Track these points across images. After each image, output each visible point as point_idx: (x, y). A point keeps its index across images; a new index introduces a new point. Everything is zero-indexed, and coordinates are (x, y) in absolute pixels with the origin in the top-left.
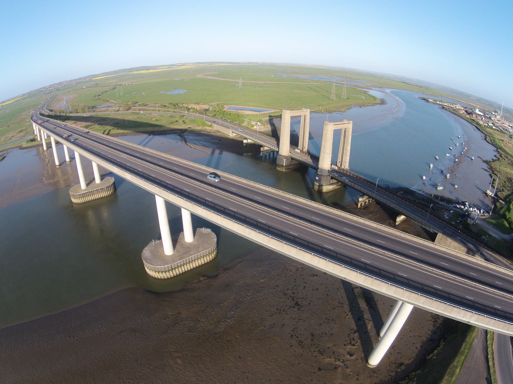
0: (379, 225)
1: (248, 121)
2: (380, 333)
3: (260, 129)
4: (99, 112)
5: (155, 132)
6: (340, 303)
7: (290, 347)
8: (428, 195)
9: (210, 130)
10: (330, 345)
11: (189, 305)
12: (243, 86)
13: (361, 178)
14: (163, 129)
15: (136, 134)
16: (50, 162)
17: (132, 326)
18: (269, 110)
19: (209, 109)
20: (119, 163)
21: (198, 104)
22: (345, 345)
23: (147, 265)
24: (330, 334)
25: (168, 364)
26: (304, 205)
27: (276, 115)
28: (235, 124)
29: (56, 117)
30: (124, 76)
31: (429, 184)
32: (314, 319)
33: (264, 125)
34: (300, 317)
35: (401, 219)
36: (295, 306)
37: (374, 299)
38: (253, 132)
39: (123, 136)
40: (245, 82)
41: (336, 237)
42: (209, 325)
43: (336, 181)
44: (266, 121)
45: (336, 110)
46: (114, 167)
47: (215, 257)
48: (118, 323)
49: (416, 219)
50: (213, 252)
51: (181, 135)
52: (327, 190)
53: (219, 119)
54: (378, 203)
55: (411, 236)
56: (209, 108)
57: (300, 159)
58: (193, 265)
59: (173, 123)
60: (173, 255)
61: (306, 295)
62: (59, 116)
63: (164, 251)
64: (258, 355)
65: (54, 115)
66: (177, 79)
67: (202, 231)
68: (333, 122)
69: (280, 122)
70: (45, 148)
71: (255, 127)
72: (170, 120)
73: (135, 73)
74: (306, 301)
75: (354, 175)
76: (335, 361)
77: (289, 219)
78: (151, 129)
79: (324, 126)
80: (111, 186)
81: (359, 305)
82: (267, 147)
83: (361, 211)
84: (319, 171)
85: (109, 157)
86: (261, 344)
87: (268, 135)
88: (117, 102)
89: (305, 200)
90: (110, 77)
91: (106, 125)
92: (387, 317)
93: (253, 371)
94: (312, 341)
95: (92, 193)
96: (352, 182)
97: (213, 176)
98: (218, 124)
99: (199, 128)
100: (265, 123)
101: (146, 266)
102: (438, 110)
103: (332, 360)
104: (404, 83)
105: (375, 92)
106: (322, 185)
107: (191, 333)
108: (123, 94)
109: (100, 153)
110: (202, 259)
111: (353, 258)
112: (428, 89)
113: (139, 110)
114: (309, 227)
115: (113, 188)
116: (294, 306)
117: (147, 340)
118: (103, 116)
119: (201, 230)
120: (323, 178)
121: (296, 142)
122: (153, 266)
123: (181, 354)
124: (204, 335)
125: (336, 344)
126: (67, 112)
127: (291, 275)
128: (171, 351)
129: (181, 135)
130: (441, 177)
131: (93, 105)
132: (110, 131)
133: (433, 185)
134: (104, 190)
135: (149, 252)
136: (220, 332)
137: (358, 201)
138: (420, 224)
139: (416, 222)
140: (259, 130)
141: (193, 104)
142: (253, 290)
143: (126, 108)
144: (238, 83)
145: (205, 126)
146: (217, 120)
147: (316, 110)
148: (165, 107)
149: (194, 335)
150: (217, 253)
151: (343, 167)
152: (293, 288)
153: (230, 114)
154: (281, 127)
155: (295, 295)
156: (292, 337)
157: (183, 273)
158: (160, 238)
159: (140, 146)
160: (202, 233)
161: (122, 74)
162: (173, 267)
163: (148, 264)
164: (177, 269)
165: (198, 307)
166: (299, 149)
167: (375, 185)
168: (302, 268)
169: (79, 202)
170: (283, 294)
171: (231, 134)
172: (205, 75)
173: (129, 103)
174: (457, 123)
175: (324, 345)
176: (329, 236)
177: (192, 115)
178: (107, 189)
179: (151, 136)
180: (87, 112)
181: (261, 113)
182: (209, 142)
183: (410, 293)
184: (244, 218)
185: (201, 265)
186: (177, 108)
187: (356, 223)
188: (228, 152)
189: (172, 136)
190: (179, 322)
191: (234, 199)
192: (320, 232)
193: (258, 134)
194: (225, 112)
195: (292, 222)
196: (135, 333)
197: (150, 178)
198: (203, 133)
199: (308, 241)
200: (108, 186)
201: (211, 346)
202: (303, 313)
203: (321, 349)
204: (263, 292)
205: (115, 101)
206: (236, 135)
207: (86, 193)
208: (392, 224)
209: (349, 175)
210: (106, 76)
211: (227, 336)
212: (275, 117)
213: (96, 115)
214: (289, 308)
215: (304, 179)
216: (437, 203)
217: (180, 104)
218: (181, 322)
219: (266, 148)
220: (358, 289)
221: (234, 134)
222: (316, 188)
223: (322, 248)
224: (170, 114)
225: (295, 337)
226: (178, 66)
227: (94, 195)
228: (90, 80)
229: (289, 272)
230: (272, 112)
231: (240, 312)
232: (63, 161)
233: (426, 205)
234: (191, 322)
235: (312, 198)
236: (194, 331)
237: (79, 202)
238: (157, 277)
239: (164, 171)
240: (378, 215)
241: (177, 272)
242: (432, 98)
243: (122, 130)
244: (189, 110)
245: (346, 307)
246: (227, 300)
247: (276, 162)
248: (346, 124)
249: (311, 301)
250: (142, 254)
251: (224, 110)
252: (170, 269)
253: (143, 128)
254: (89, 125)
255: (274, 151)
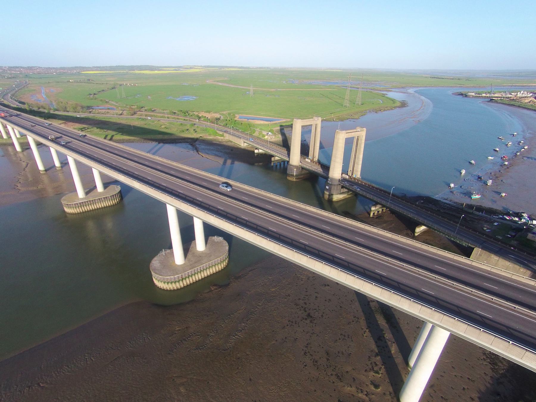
0: (394, 235)
1: (260, 130)
2: (409, 361)
3: (271, 139)
4: (97, 114)
5: (165, 140)
6: (355, 317)
7: (304, 368)
8: (458, 204)
9: (222, 140)
10: (349, 369)
11: (198, 318)
12: (254, 93)
13: (373, 187)
14: (173, 138)
15: (143, 141)
16: (28, 166)
17: (131, 349)
18: (280, 120)
19: (220, 118)
20: (125, 171)
21: (209, 112)
22: (366, 370)
23: (156, 276)
24: (347, 354)
25: (168, 396)
26: (315, 214)
27: (287, 124)
28: (247, 134)
29: (32, 112)
30: (125, 75)
31: (459, 192)
32: (328, 334)
33: (275, 134)
34: (313, 331)
35: (421, 230)
36: (308, 318)
37: (395, 317)
38: (264, 142)
39: (129, 142)
40: (256, 90)
41: (347, 246)
42: (218, 340)
43: (346, 190)
44: (277, 131)
45: (349, 117)
46: (120, 175)
47: (226, 265)
48: (114, 348)
49: (440, 231)
50: (225, 260)
51: (192, 144)
52: (338, 199)
53: (231, 129)
54: (393, 212)
55: (435, 249)
56: (220, 117)
57: (311, 168)
58: (207, 273)
59: (183, 132)
60: (184, 264)
61: (319, 307)
62: (37, 111)
63: (174, 261)
64: (270, 377)
65: (27, 109)
66: (186, 84)
67: (214, 240)
68: (345, 130)
69: (290, 132)
70: (18, 148)
71: (266, 137)
72: (181, 128)
73: (137, 72)
74: (319, 313)
75: (367, 184)
76: (357, 391)
77: (299, 228)
78: (160, 137)
79: (336, 134)
80: (116, 195)
81: (377, 321)
82: (278, 157)
83: (374, 220)
84: (329, 180)
85: (113, 164)
86: (273, 362)
87: (279, 145)
88: (118, 105)
89: (315, 209)
90: (106, 73)
91: (108, 129)
92: (415, 341)
93: (264, 399)
94: (327, 361)
95: (93, 202)
96: (364, 190)
97: (225, 185)
98: (230, 134)
99: (210, 137)
100: (276, 133)
101: (154, 277)
102: (482, 105)
103: (353, 389)
104: (435, 78)
105: (395, 93)
106: (332, 195)
107: (199, 350)
108: (125, 97)
109: (102, 160)
110: (213, 267)
111: (367, 269)
112: (470, 79)
113: (146, 116)
114: (319, 235)
115: (119, 197)
116: (306, 317)
117: (147, 366)
118: (103, 119)
119: (213, 239)
120: (333, 187)
121: (307, 151)
122: (162, 277)
123: (185, 380)
124: (213, 352)
125: (356, 369)
126: (50, 109)
127: (302, 284)
128: (174, 376)
129: (192, 144)
130: (477, 185)
131: (89, 105)
132: (113, 136)
133: (465, 194)
134: (108, 199)
135: (158, 262)
136: (230, 348)
137: (371, 210)
138: (447, 237)
139: (442, 234)
140: (270, 140)
141: (203, 112)
142: (264, 299)
143: (130, 113)
144: (249, 91)
145: (216, 135)
146: (228, 130)
147: (328, 118)
148: (175, 114)
149: (202, 353)
150: (229, 261)
151: (354, 176)
152: (305, 298)
153: (242, 123)
154: (291, 137)
155: (307, 306)
156: (305, 355)
157: (193, 283)
158: (170, 247)
159: (149, 154)
160: (214, 241)
161: (122, 72)
162: (184, 277)
163: (156, 275)
164: (187, 279)
165: (208, 319)
166: (309, 159)
167: (389, 194)
168: (313, 277)
169: (75, 212)
170: (294, 304)
171: (243, 144)
172: (215, 81)
173: (133, 106)
174: (513, 117)
175: (342, 368)
176: (340, 245)
177: (203, 123)
178: (111, 198)
179: (161, 144)
180: (80, 112)
181: (272, 122)
182: (221, 152)
183: (442, 315)
184: (255, 226)
185: (212, 274)
186: (187, 116)
187: (368, 232)
188: (240, 162)
189: (184, 145)
190: (186, 338)
191: (246, 207)
192: (330, 241)
193: (269, 144)
194: (237, 121)
195: (302, 230)
196: (134, 357)
197: (161, 187)
198: (215, 142)
199: (319, 249)
200: (113, 195)
201: (219, 366)
202: (315, 326)
203: (339, 373)
204: (275, 301)
205: (117, 103)
206: (248, 145)
207: (85, 202)
208: (410, 234)
209: (360, 184)
210: (101, 71)
211: (237, 352)
212: (285, 127)
213: (94, 116)
214: (302, 320)
215: (314, 187)
216: (472, 213)
217: (190, 112)
218: (189, 339)
219: (277, 158)
220: (374, 303)
221: (246, 144)
222: (326, 197)
223: (333, 257)
224: (180, 122)
225: (308, 354)
226: (186, 68)
227: (96, 204)
228: (78, 72)
229: (300, 281)
230: (284, 121)
231: (251, 324)
232: (50, 166)
233: (454, 215)
234: (199, 337)
235: (322, 206)
236: (202, 347)
237: (75, 212)
238: (166, 288)
239: (175, 180)
240: (393, 225)
241: (188, 282)
242: (475, 90)
243: (127, 136)
244: (200, 118)
245: (363, 323)
246: (238, 310)
247: (287, 172)
248: (359, 131)
249: (323, 313)
250: (151, 264)
251: (235, 119)
252: (180, 279)
253: (152, 136)
254: (84, 128)
255: (285, 161)
